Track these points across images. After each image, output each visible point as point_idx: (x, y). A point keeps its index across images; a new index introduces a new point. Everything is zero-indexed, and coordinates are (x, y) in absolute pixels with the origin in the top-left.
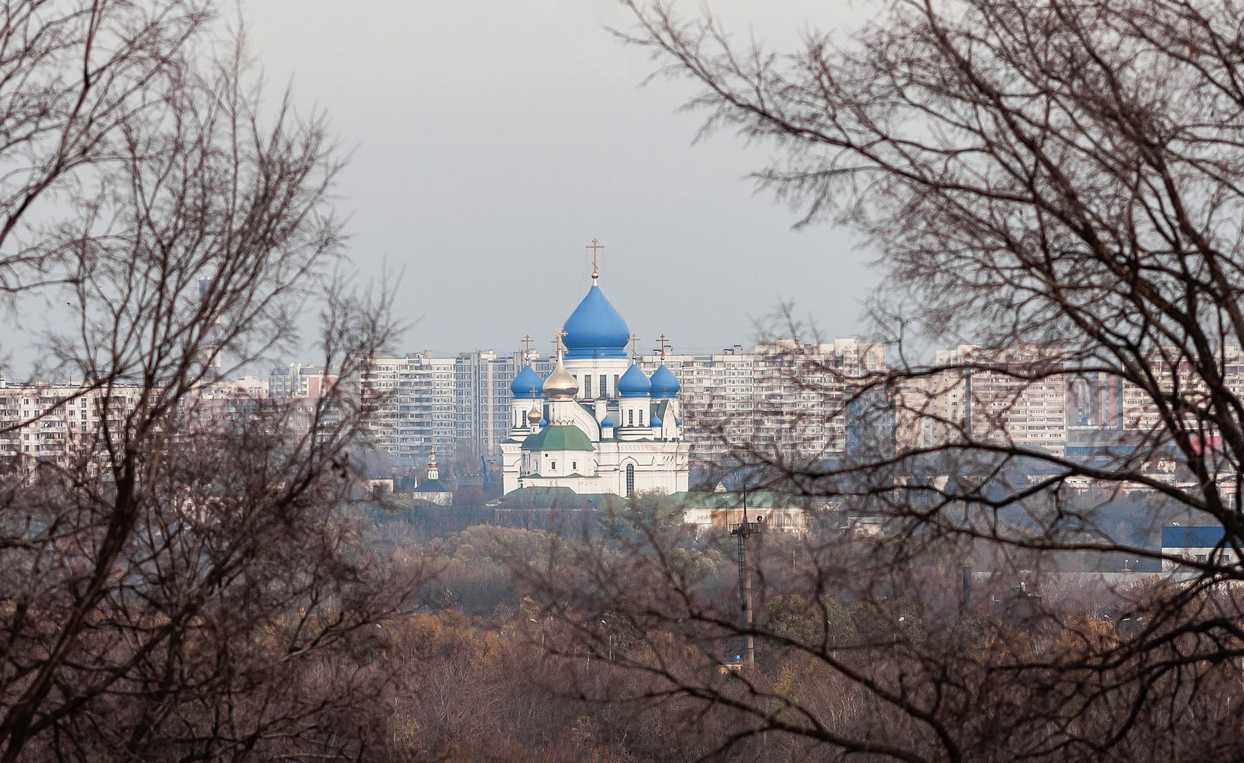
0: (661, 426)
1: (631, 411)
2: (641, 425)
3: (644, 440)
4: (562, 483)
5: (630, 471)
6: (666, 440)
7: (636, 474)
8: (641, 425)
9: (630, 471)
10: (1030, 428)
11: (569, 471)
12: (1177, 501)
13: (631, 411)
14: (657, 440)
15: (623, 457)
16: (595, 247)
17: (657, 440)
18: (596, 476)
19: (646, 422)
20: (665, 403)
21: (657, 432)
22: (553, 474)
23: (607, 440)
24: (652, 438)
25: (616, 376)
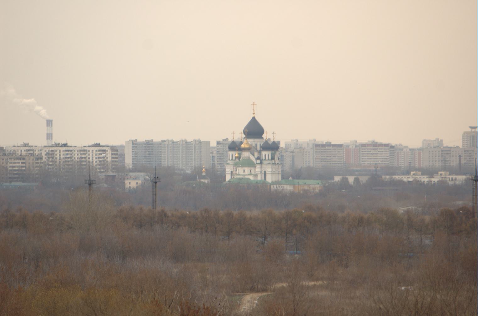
19: (270, 158)
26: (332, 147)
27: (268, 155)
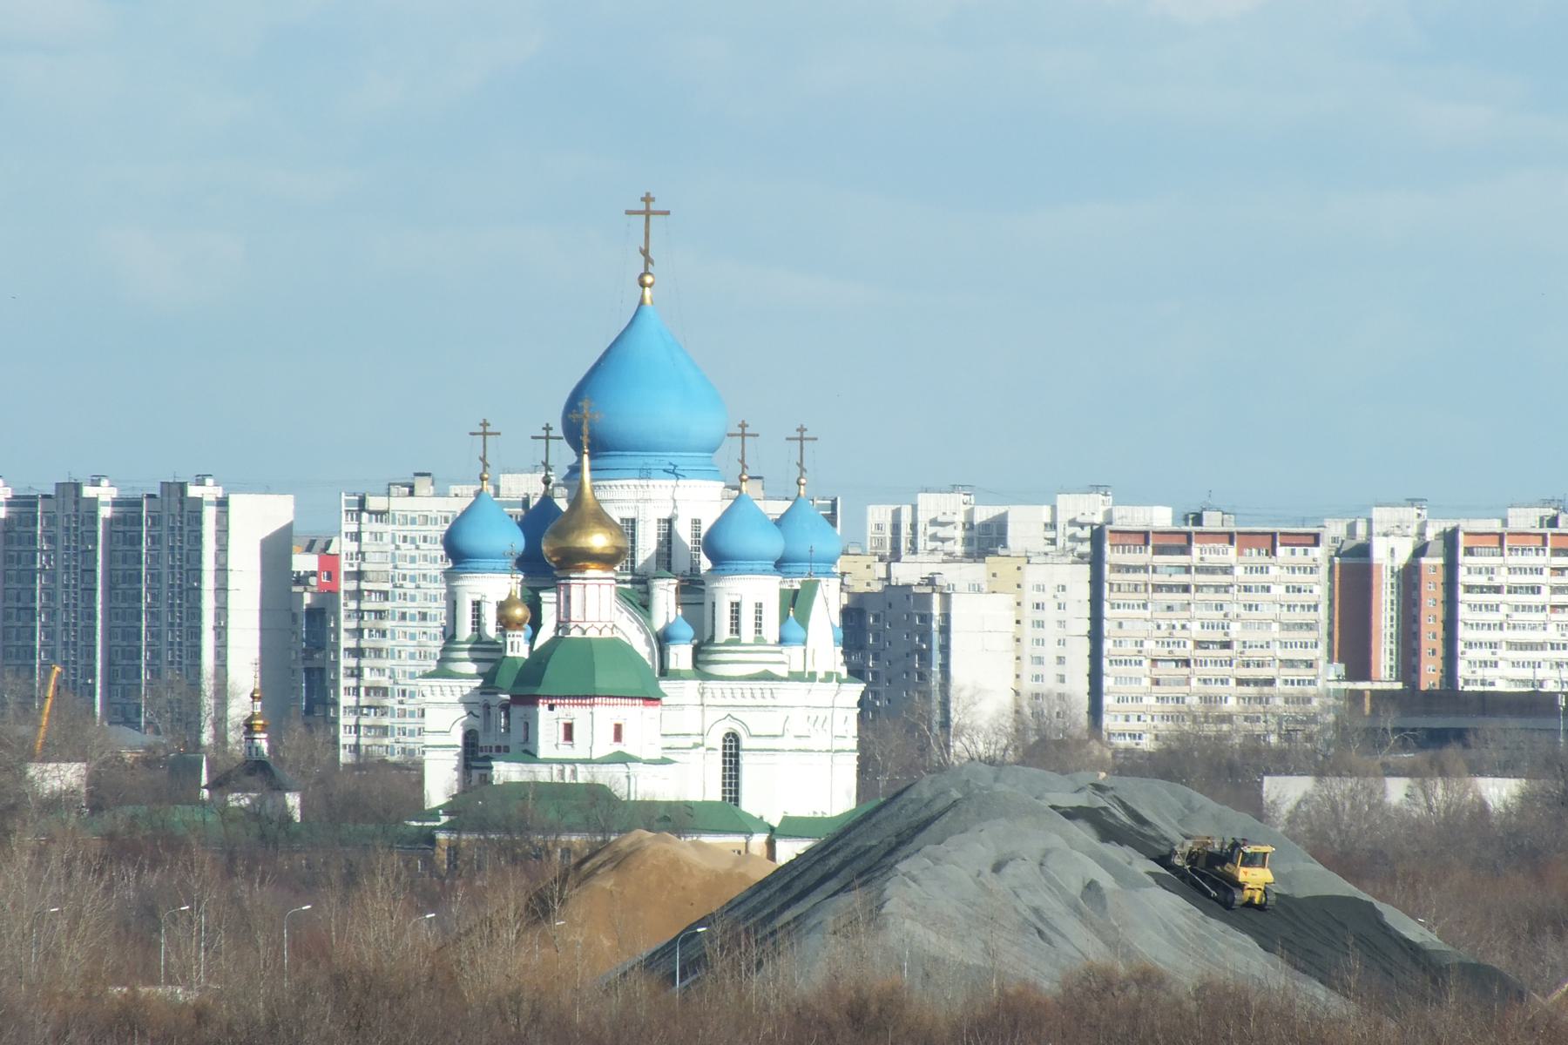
0: (805, 643)
1: (477, 605)
2: (759, 641)
3: (767, 677)
4: (583, 775)
5: (732, 750)
6: (812, 677)
7: (746, 760)
8: (759, 641)
9: (732, 750)
10: (1158, 588)
11: (605, 746)
12: (1440, 607)
13: (759, 606)
14: (795, 677)
15: (712, 715)
16: (648, 213)
17: (795, 677)
18: (664, 761)
19: (771, 630)
20: (810, 588)
21: (793, 657)
22: (565, 752)
23: (678, 675)
24: (782, 671)
25: (696, 523)
26: (1240, 553)
27: (759, 606)
